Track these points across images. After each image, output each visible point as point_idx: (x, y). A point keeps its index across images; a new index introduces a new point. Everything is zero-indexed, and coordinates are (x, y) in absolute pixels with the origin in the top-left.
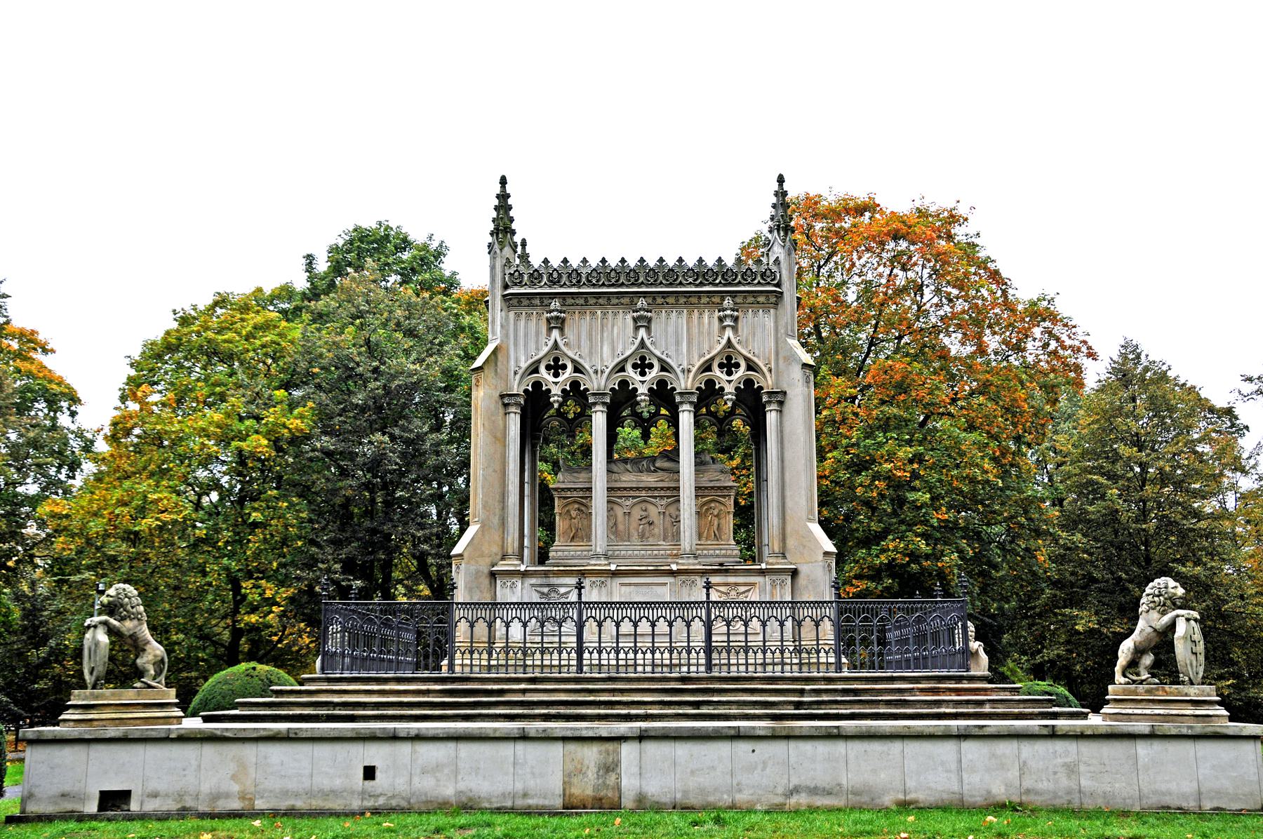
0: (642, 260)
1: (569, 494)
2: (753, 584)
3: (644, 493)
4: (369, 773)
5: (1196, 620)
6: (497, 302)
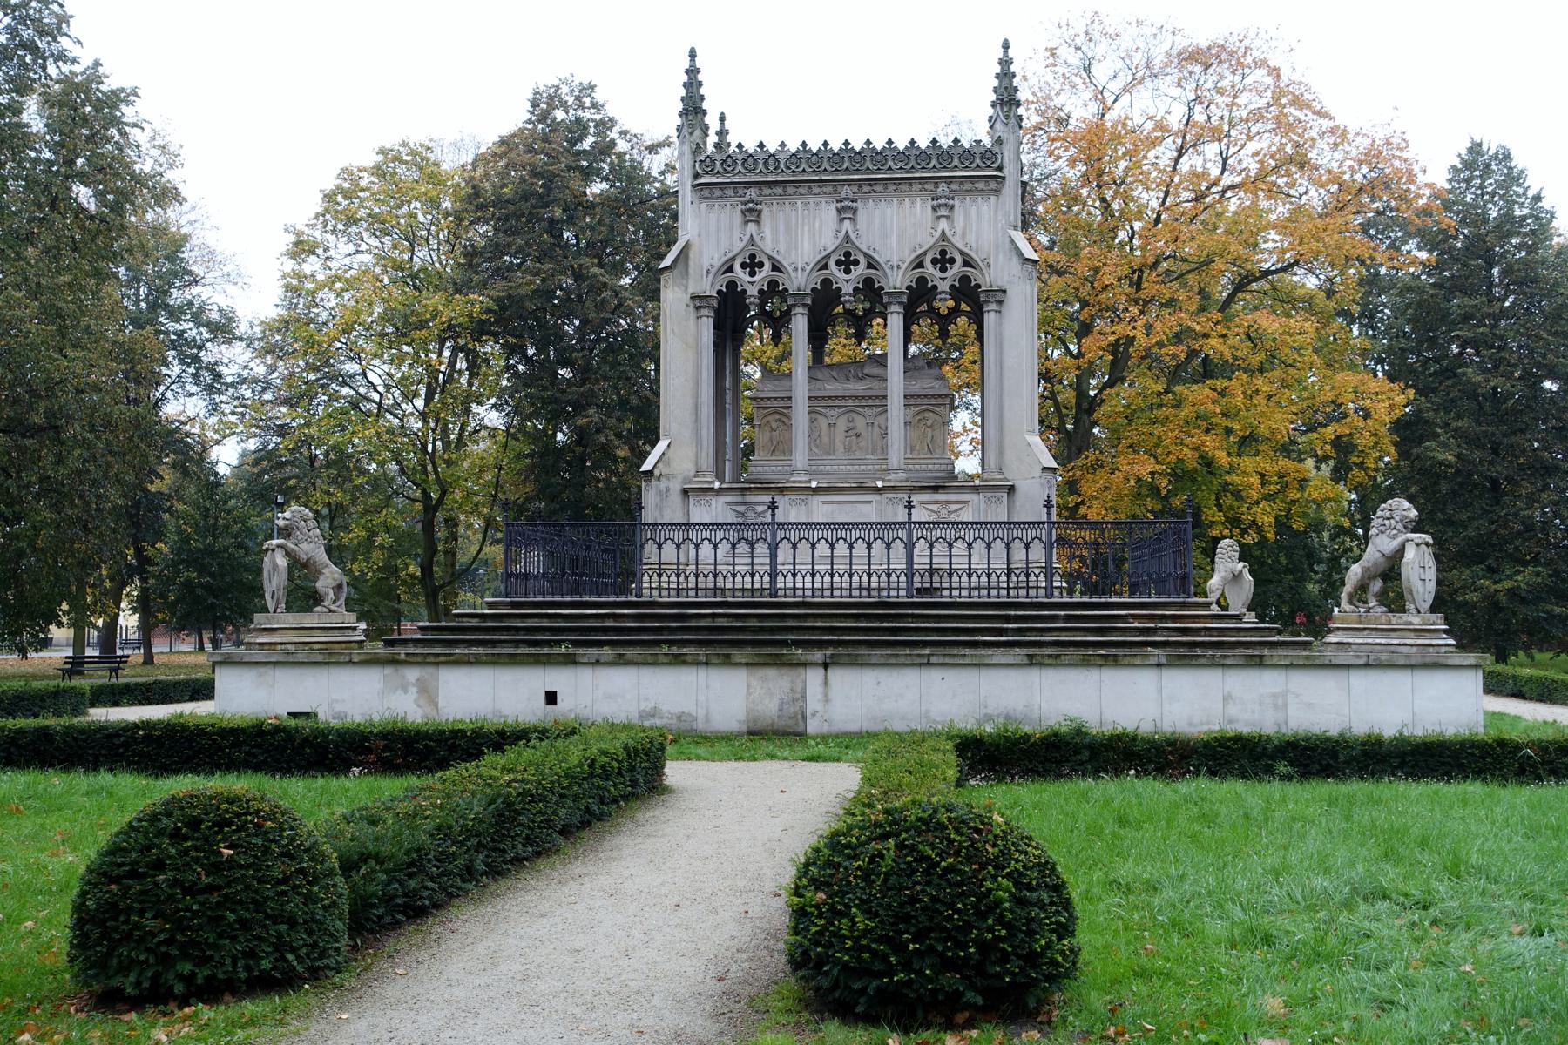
0: (847, 143)
1: (769, 404)
2: (966, 502)
3: (850, 402)
4: (551, 698)
5: (1427, 545)
6: (686, 195)
